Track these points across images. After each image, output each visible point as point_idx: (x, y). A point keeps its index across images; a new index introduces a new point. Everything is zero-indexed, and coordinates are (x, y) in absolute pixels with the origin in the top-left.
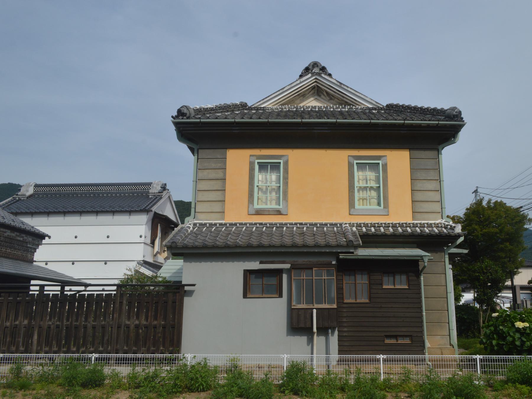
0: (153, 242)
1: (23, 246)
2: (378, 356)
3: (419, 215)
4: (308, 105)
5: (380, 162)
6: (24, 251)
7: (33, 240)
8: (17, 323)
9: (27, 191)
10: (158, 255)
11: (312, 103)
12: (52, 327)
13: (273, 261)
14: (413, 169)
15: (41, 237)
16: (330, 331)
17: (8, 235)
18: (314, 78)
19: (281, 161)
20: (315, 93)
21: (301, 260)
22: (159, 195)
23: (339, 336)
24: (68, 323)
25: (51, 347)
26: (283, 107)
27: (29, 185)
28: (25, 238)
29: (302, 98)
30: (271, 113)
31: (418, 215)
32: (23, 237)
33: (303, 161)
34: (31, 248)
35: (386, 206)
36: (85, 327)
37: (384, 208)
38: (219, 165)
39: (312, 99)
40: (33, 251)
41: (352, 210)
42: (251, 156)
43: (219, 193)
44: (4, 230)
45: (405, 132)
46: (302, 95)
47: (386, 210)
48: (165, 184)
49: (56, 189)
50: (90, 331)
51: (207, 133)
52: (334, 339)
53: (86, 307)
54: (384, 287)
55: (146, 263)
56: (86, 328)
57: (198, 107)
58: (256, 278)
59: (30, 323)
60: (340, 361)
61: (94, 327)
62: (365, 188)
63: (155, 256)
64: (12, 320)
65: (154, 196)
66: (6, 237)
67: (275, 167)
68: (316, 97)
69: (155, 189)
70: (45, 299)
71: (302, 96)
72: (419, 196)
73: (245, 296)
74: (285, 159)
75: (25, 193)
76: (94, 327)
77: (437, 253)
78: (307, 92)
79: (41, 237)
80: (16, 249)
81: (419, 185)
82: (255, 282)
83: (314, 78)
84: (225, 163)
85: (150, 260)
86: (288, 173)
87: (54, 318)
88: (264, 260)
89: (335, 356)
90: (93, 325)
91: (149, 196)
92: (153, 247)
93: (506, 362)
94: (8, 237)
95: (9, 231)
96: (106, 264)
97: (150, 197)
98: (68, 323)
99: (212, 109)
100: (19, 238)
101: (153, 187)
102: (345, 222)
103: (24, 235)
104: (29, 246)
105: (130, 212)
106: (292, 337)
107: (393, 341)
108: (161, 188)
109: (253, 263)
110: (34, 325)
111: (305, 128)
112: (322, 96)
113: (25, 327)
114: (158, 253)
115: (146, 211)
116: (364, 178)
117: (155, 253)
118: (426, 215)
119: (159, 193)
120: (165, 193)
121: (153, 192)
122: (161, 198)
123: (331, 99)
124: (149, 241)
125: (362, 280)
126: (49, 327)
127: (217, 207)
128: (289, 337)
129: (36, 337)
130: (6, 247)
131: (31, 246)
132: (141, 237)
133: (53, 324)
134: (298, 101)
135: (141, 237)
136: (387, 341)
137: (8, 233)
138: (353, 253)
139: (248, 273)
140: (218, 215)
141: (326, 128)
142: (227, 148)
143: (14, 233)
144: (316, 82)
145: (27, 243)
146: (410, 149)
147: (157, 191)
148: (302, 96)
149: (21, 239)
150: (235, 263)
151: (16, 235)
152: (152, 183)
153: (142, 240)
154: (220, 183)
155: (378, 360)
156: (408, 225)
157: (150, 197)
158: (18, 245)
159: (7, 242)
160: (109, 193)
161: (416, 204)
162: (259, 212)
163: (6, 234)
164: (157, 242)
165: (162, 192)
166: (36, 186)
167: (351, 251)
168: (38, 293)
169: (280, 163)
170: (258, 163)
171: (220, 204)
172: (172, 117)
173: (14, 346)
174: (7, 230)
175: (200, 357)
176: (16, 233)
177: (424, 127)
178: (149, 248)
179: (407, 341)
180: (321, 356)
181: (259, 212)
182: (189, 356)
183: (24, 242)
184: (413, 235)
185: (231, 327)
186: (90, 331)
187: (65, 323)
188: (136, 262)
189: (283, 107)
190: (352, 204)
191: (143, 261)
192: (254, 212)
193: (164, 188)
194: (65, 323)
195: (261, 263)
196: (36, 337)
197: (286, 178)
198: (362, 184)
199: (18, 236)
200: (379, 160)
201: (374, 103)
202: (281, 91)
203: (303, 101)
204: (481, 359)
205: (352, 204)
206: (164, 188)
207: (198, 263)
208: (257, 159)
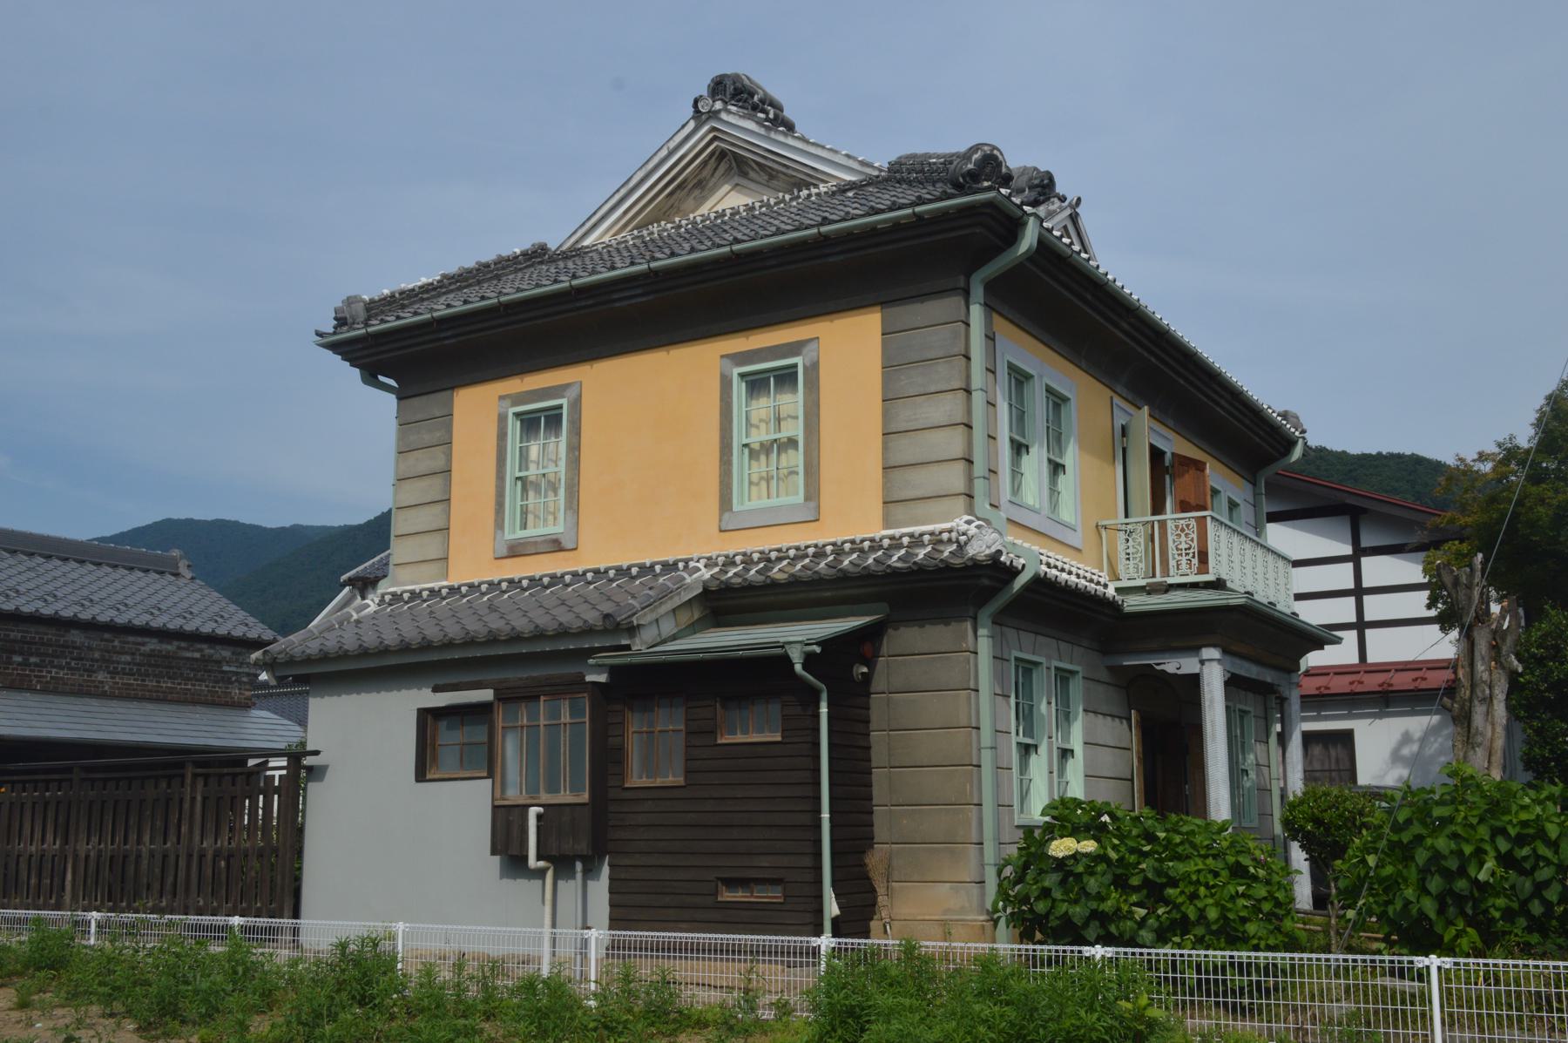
2: (1420, 961)
3: (899, 508)
4: (719, 208)
5: (798, 360)
6: (217, 682)
11: (729, 199)
13: (493, 679)
14: (892, 366)
16: (579, 866)
18: (706, 128)
19: (564, 402)
20: (730, 169)
21: (515, 675)
23: (611, 879)
26: (645, 233)
29: (697, 192)
30: (607, 255)
31: (899, 511)
32: (200, 650)
33: (627, 395)
35: (813, 492)
37: (807, 498)
38: (438, 435)
39: (727, 187)
41: (726, 516)
42: (502, 398)
43: (437, 509)
44: (140, 639)
45: (841, 257)
46: (690, 183)
47: (812, 504)
51: (420, 350)
52: (600, 889)
54: (724, 739)
57: (386, 292)
58: (449, 728)
60: (614, 946)
62: (766, 448)
67: (786, 378)
68: (737, 179)
71: (695, 186)
72: (907, 450)
73: (421, 776)
74: (809, 351)
77: (947, 624)
78: (706, 173)
80: (189, 679)
81: (908, 415)
82: (449, 737)
83: (706, 128)
84: (449, 428)
86: (579, 434)
88: (441, 681)
89: (598, 935)
93: (1301, 975)
94: (152, 654)
95: (155, 640)
99: (427, 289)
100: (189, 655)
102: (695, 556)
103: (204, 646)
104: (225, 668)
106: (510, 881)
107: (739, 896)
109: (414, 692)
111: (590, 302)
112: (752, 174)
116: (761, 416)
118: (920, 509)
123: (771, 177)
125: (669, 722)
127: (431, 547)
128: (505, 881)
134: (690, 202)
136: (727, 896)
137: (152, 645)
138: (628, 647)
139: (428, 719)
140: (434, 567)
141: (639, 291)
142: (453, 388)
144: (715, 138)
146: (884, 303)
148: (695, 186)
149: (197, 655)
150: (404, 692)
151: (179, 648)
154: (437, 481)
155: (1423, 975)
156: (875, 545)
159: (157, 666)
161: (896, 474)
162: (516, 551)
163: (146, 649)
167: (624, 642)
168: (284, 772)
169: (795, 366)
170: (742, 376)
171: (438, 538)
172: (319, 334)
175: (353, 928)
176: (176, 643)
177: (884, 232)
179: (773, 895)
180: (565, 933)
181: (516, 551)
182: (324, 927)
183: (205, 660)
184: (843, 579)
185: (402, 855)
189: (645, 233)
190: (725, 502)
192: (505, 552)
195: (436, 689)
197: (574, 449)
198: (759, 436)
199: (187, 649)
200: (797, 354)
201: (856, 166)
202: (623, 191)
203: (704, 199)
204: (1448, 971)
205: (725, 502)
207: (354, 696)
208: (515, 404)
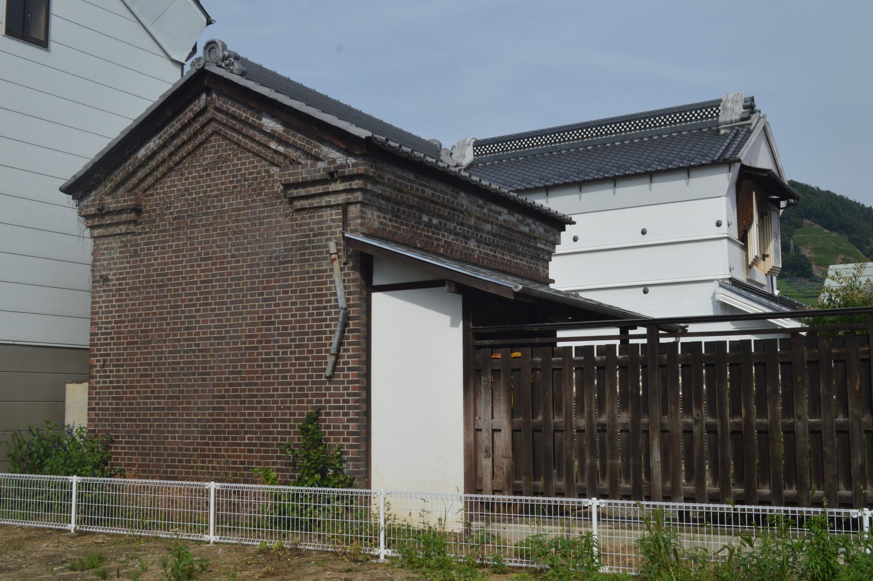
0: (743, 237)
1: (529, 246)
7: (546, 231)
8: (604, 419)
9: (463, 156)
10: (754, 267)
12: (696, 429)
15: (559, 223)
17: (505, 221)
22: (743, 126)
24: (738, 420)
25: (548, 480)
27: (463, 145)
28: (533, 226)
32: (529, 225)
34: (543, 250)
36: (790, 432)
40: (546, 257)
44: (498, 209)
48: (752, 99)
49: (516, 144)
50: (804, 441)
53: (731, 380)
55: (735, 284)
56: (793, 432)
59: (635, 420)
61: (815, 432)
63: (749, 267)
64: (590, 413)
65: (732, 128)
66: (501, 226)
69: (732, 113)
70: (665, 356)
75: (459, 161)
76: (815, 432)
79: (559, 223)
80: (518, 253)
85: (741, 276)
87: (699, 405)
90: (811, 425)
91: (718, 131)
92: (745, 248)
95: (506, 211)
96: (645, 292)
97: (722, 132)
98: (738, 420)
101: (725, 109)
103: (530, 221)
104: (539, 245)
105: (688, 170)
108: (745, 107)
110: (647, 425)
113: (627, 431)
114: (756, 260)
115: (723, 163)
117: (751, 260)
119: (742, 120)
120: (754, 118)
121: (728, 119)
122: (749, 132)
124: (735, 235)
126: (688, 431)
129: (656, 456)
130: (502, 248)
131: (542, 246)
132: (719, 224)
133: (696, 422)
135: (719, 224)
137: (505, 216)
143: (513, 216)
145: (535, 238)
147: (738, 117)
149: (527, 229)
152: (720, 100)
153: (723, 231)
157: (722, 132)
158: (521, 244)
160: (626, 137)
164: (754, 234)
165: (749, 118)
166: (478, 144)
168: (645, 341)
173: (603, 477)
174: (502, 209)
176: (516, 215)
178: (738, 251)
186: (804, 441)
187: (730, 421)
188: (716, 283)
191: (730, 279)
193: (750, 107)
194: (730, 421)
196: (656, 456)
206: (750, 107)
